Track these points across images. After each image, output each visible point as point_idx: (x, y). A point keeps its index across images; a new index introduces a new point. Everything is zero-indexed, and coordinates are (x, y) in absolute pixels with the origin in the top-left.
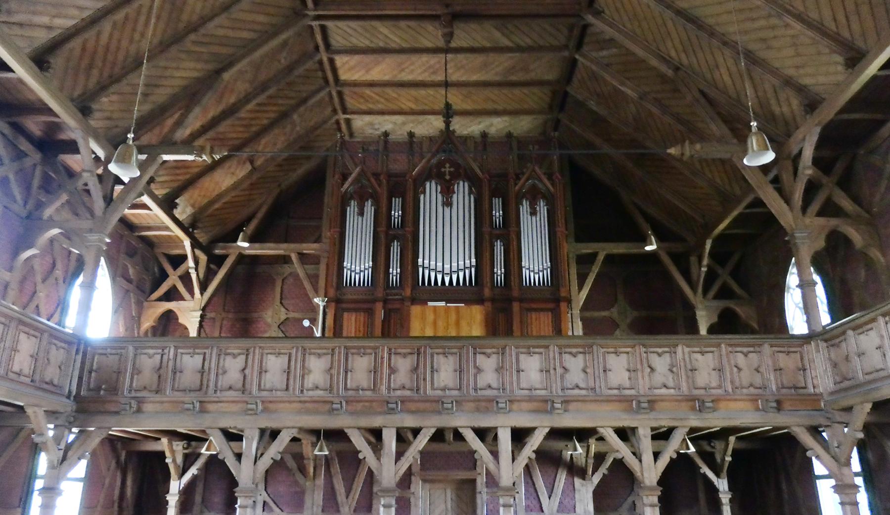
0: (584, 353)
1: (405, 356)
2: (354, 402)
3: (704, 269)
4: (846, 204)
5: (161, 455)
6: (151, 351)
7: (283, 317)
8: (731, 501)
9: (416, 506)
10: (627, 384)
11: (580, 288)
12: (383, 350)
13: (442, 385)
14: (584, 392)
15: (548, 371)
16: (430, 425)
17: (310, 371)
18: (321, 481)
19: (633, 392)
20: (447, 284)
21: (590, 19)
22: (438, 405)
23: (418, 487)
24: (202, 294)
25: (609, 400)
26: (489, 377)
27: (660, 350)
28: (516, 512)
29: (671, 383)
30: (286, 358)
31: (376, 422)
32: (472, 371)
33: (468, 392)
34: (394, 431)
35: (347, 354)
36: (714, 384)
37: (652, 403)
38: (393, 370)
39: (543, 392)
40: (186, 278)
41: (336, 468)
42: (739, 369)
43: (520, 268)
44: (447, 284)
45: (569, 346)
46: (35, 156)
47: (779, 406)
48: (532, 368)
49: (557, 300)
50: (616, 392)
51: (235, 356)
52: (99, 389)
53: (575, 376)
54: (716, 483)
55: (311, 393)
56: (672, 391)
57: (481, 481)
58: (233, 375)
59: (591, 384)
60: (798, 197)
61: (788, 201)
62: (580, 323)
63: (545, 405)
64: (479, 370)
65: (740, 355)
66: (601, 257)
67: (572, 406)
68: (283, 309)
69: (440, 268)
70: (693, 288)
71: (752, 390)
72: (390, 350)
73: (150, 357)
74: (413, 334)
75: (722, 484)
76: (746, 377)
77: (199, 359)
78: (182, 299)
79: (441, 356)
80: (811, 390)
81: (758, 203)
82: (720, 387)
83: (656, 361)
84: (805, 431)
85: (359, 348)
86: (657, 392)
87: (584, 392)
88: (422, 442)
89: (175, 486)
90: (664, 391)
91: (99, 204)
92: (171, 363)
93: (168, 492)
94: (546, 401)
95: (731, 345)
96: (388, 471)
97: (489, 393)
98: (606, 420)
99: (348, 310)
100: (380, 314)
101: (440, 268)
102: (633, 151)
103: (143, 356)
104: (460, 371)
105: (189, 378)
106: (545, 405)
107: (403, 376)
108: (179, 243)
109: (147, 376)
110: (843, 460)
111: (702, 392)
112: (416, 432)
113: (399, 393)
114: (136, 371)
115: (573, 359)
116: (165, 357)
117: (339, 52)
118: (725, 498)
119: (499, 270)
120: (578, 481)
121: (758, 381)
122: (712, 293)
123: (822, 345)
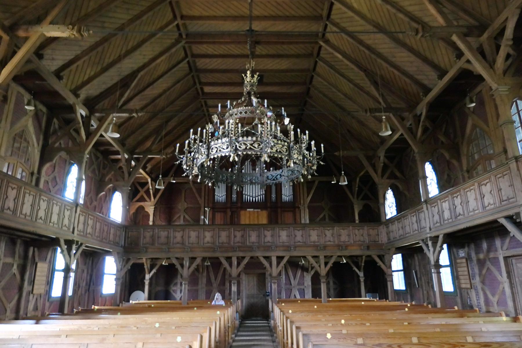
0: (302, 230)
1: (239, 231)
3: (357, 189)
4: (398, 174)
5: (143, 264)
7: (186, 207)
8: (364, 280)
9: (242, 283)
10: (317, 241)
11: (308, 196)
15: (289, 236)
16: (248, 255)
17: (206, 237)
18: (205, 274)
19: (318, 243)
21: (308, 99)
22: (251, 249)
23: (244, 277)
25: (310, 246)
26: (269, 239)
27: (329, 229)
29: (332, 240)
30: (197, 232)
31: (230, 255)
32: (263, 236)
34: (236, 258)
36: (347, 240)
37: (325, 247)
38: (235, 236)
39: (287, 244)
40: (147, 192)
41: (211, 269)
42: (356, 235)
43: (281, 195)
46: (101, 157)
47: (368, 248)
48: (284, 235)
50: (313, 243)
51: (179, 232)
52: (131, 244)
53: (299, 238)
55: (207, 245)
57: (267, 274)
58: (179, 239)
59: (304, 240)
60: (380, 171)
61: (376, 173)
62: (307, 210)
64: (265, 236)
65: (356, 230)
66: (316, 183)
67: (297, 249)
68: (186, 203)
69: (251, 195)
70: (353, 195)
71: (360, 242)
73: (148, 232)
74: (243, 222)
75: (361, 274)
76: (357, 238)
77: (166, 233)
78: (147, 201)
80: (380, 242)
81: (367, 172)
82: (349, 241)
83: (327, 232)
88: (245, 261)
89: (148, 277)
90: (329, 243)
91: (126, 175)
92: (157, 235)
96: (234, 271)
97: (269, 244)
98: (309, 253)
99: (217, 212)
100: (229, 213)
101: (251, 195)
104: (259, 236)
105: (163, 240)
106: (288, 248)
107: (238, 239)
108: (147, 179)
109: (148, 239)
110: (388, 266)
112: (243, 258)
113: (237, 244)
114: (144, 237)
115: (298, 232)
117: (210, 107)
118: (362, 280)
119: (274, 196)
120: (305, 273)
121: (362, 239)
122: (360, 198)
123: (385, 227)
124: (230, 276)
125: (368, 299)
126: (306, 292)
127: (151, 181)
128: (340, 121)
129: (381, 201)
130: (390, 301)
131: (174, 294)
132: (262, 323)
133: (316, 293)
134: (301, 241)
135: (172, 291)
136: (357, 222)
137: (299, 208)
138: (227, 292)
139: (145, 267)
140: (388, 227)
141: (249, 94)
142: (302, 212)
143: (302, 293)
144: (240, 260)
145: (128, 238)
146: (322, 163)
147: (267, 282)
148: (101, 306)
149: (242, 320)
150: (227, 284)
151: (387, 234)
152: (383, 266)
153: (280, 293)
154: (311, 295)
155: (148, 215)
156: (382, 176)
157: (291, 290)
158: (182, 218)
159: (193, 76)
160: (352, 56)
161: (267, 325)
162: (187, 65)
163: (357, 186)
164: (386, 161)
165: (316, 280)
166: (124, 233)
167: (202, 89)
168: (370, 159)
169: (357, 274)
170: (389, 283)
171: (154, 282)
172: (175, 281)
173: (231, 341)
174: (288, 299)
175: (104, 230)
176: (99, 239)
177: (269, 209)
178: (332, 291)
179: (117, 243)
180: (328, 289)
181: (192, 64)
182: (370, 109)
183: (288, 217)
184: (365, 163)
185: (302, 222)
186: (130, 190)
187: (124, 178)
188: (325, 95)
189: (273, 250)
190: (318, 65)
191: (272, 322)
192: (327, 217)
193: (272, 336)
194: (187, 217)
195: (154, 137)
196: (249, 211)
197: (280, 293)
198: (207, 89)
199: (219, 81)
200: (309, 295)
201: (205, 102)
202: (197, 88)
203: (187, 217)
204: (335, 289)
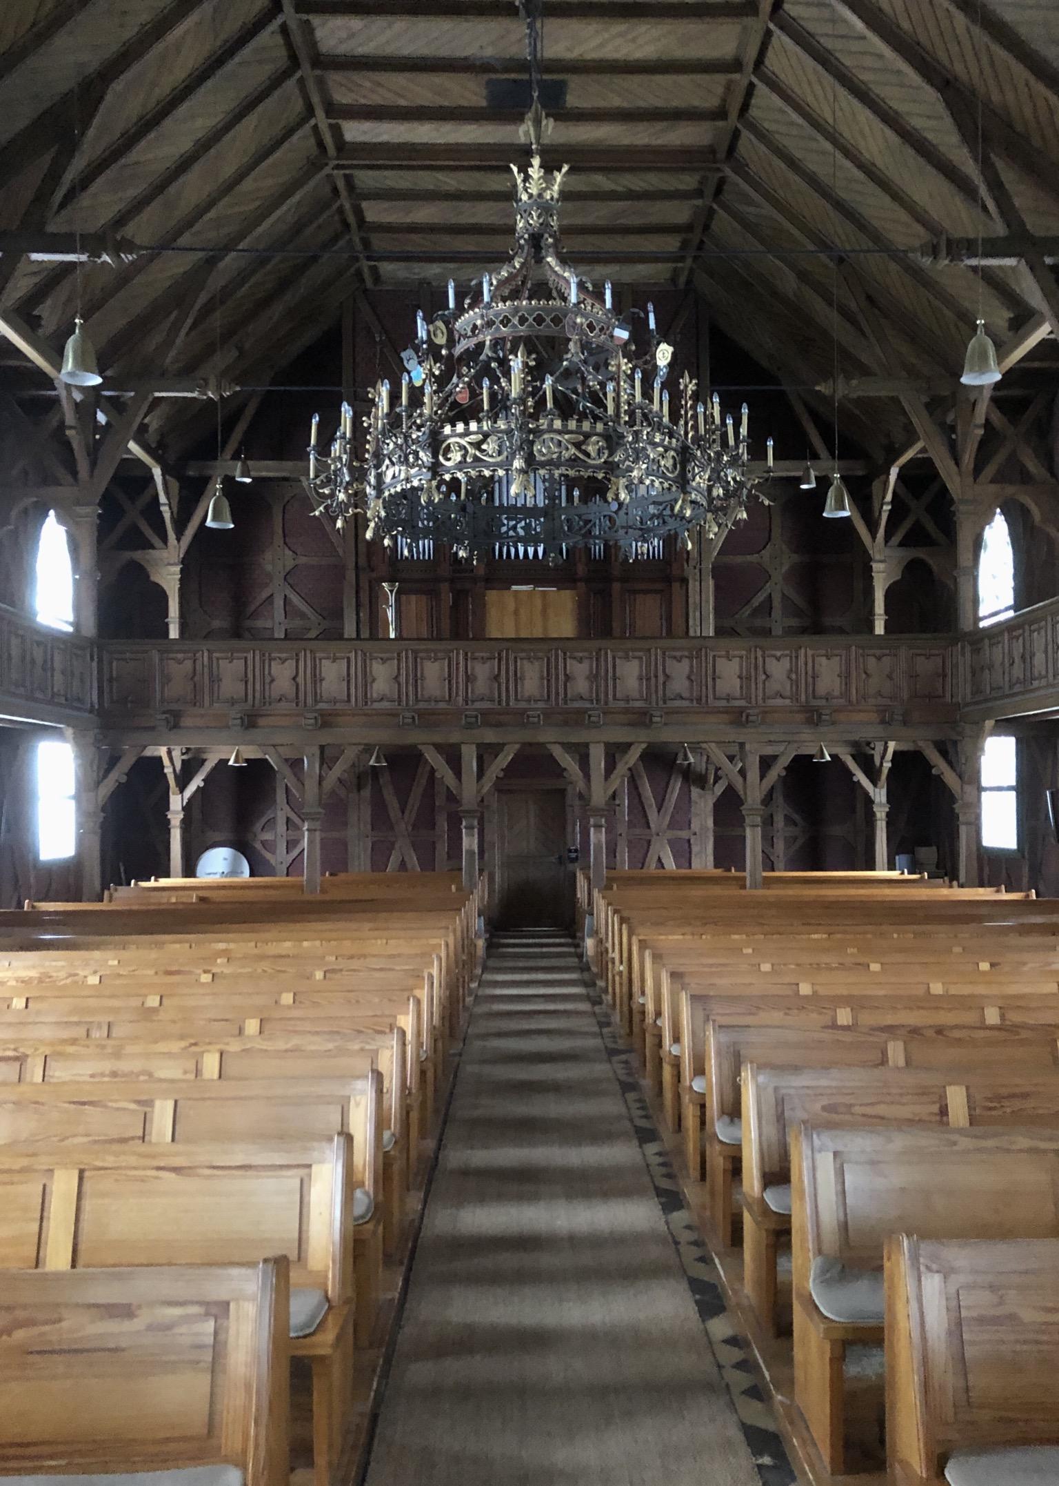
2: (427, 718)
3: (887, 508)
4: (1033, 466)
6: (180, 656)
7: (290, 564)
8: (888, 815)
12: (458, 654)
13: (527, 694)
14: (686, 703)
20: (531, 556)
21: (728, 172)
22: (521, 718)
24: (178, 540)
27: (778, 654)
28: (4, 1084)
31: (454, 738)
33: (557, 704)
35: (416, 659)
38: (469, 679)
41: (385, 779)
44: (531, 556)
45: (674, 649)
49: (668, 580)
54: (871, 794)
56: (787, 702)
60: (968, 458)
62: (711, 582)
63: (642, 719)
68: (288, 552)
72: (466, 654)
75: (879, 795)
78: (153, 547)
79: (525, 662)
84: (932, 746)
85: (427, 651)
86: (771, 702)
87: (686, 703)
89: (177, 802)
93: (168, 809)
94: (645, 714)
95: (863, 648)
97: (578, 705)
102: (772, 388)
103: (171, 662)
109: (178, 687)
111: (823, 702)
113: (478, 705)
114: (167, 679)
116: (199, 663)
118: (881, 813)
120: (695, 792)
122: (896, 540)
124: (452, 798)
125: (895, 874)
126: (695, 849)
127: (163, 475)
128: (841, 260)
129: (964, 558)
130: (961, 886)
131: (268, 855)
132: (557, 944)
133: (728, 852)
134: (686, 694)
135: (258, 846)
136: (879, 629)
137: (684, 581)
138: (442, 848)
139: (168, 770)
140: (977, 651)
141: (536, 240)
142: (693, 586)
143: (684, 853)
144: (486, 753)
145: (111, 680)
146: (767, 502)
147: (569, 816)
148: (89, 900)
149: (492, 936)
150: (443, 824)
151: (973, 674)
152: (950, 778)
153: (612, 851)
154: (711, 858)
155: (163, 596)
156: (887, 538)
157: (649, 842)
158: (279, 602)
159: (301, 81)
160: (905, 25)
161: (572, 950)
162: (279, 40)
163: (889, 498)
164: (997, 418)
165: (729, 809)
166: (95, 664)
167: (337, 131)
168: (936, 406)
169: (866, 794)
170: (963, 830)
171: (197, 814)
172: (269, 815)
173: (469, 1000)
174: (637, 872)
175: (33, 661)
176: (21, 691)
177: (581, 585)
178: (780, 846)
179: (79, 700)
180: (769, 840)
181: (297, 39)
182: (949, 242)
183: (648, 610)
184: (920, 420)
185: (691, 633)
186: (100, 516)
187: (74, 474)
188: (792, 163)
189: (596, 725)
190: (774, 40)
191: (590, 943)
192: (777, 603)
193: (589, 984)
194: (295, 599)
195: (46, 160)
196: (516, 591)
197: (612, 851)
198: (355, 131)
199: (403, 102)
200: (704, 860)
201: (349, 180)
202: (315, 127)
203: (295, 599)
204: (790, 841)
